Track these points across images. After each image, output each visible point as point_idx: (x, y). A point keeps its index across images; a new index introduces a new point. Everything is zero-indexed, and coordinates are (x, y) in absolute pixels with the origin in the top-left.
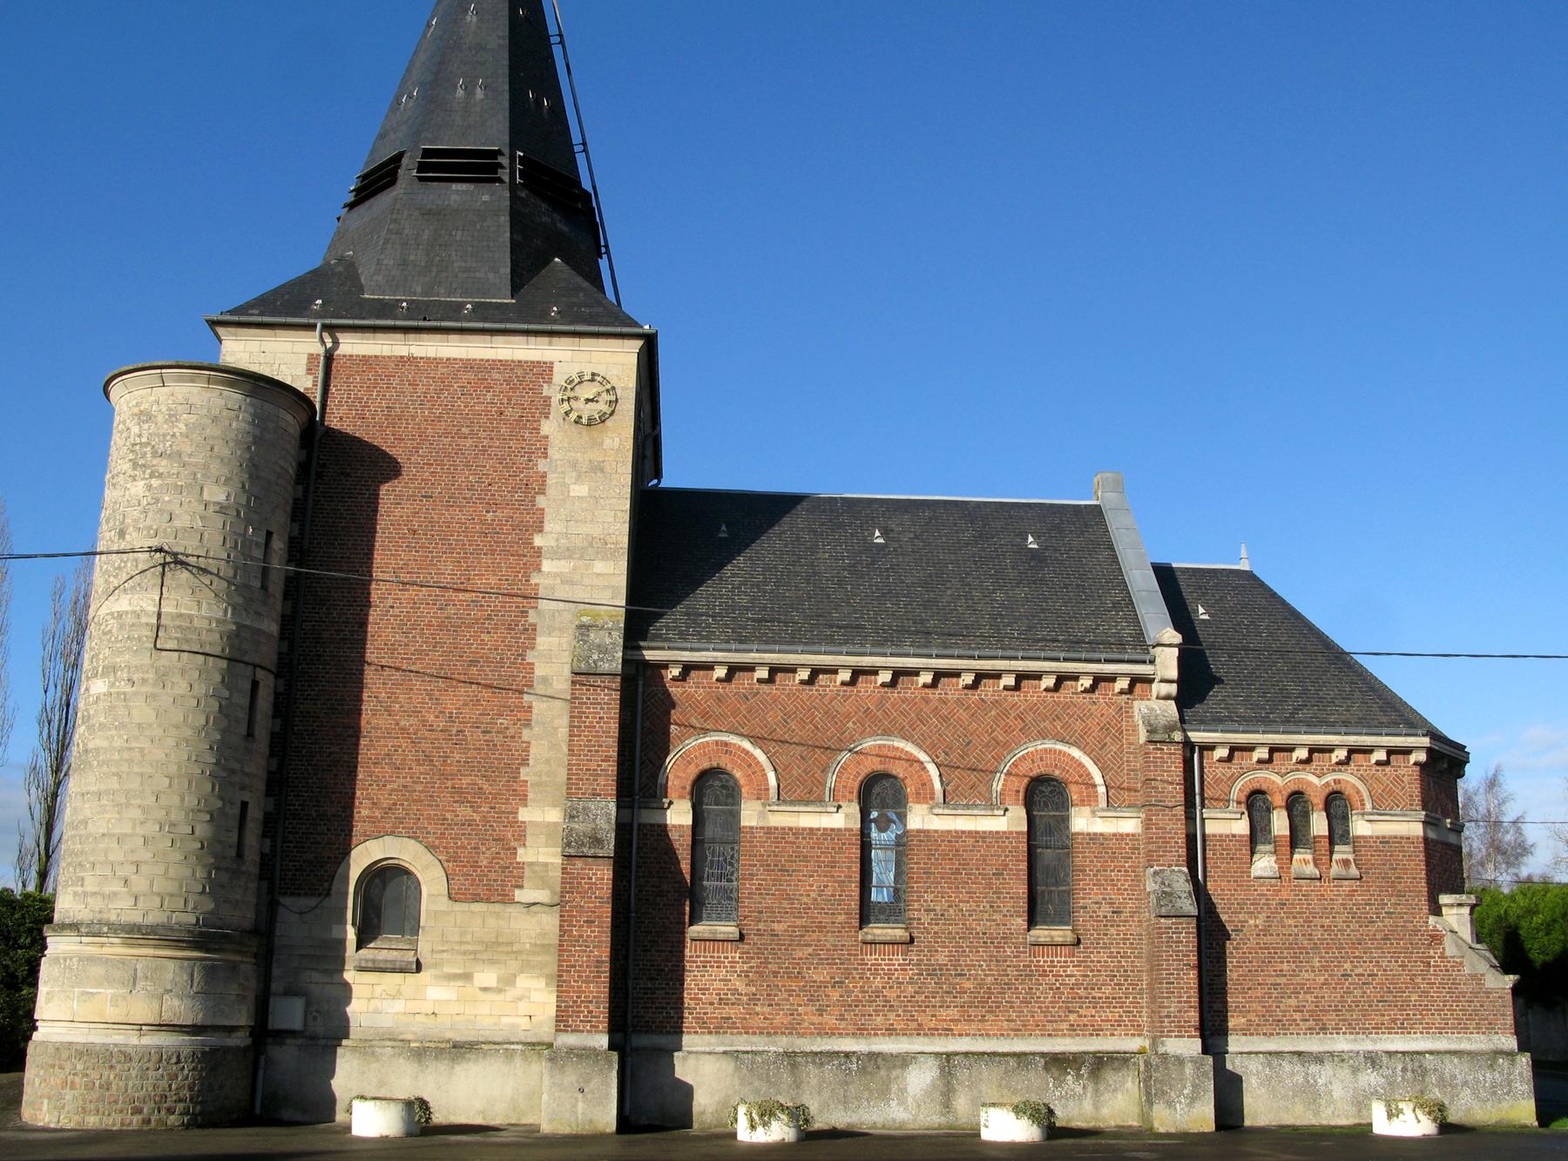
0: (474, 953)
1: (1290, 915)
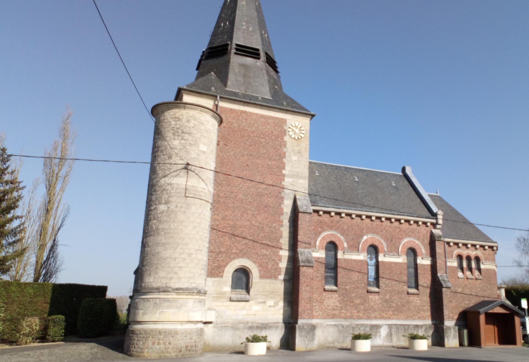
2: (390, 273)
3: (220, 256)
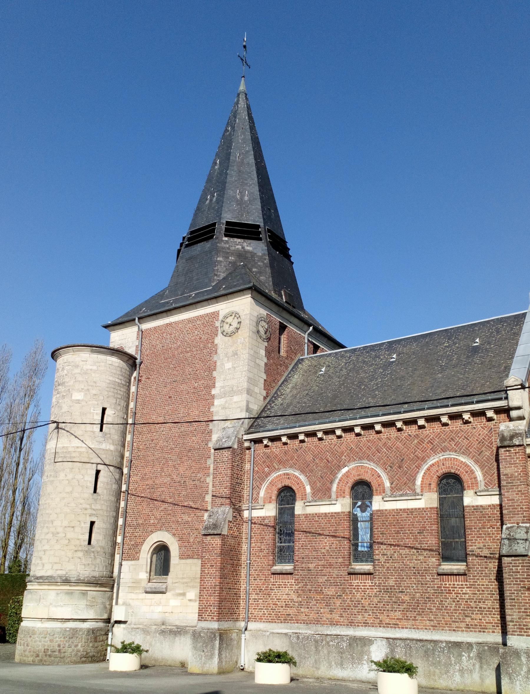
0: (186, 583)
2: (398, 533)
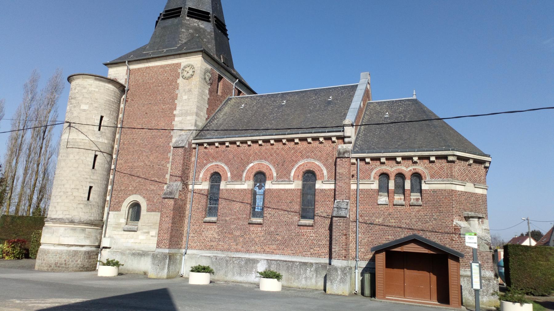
1: (392, 218)
3: (120, 193)
